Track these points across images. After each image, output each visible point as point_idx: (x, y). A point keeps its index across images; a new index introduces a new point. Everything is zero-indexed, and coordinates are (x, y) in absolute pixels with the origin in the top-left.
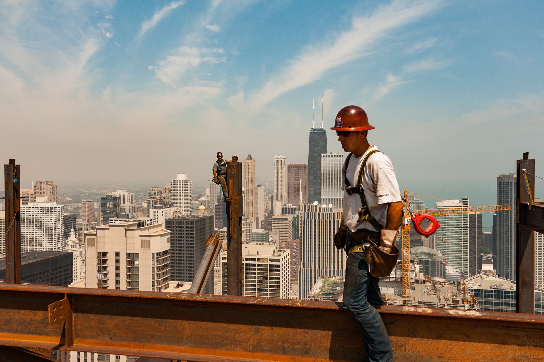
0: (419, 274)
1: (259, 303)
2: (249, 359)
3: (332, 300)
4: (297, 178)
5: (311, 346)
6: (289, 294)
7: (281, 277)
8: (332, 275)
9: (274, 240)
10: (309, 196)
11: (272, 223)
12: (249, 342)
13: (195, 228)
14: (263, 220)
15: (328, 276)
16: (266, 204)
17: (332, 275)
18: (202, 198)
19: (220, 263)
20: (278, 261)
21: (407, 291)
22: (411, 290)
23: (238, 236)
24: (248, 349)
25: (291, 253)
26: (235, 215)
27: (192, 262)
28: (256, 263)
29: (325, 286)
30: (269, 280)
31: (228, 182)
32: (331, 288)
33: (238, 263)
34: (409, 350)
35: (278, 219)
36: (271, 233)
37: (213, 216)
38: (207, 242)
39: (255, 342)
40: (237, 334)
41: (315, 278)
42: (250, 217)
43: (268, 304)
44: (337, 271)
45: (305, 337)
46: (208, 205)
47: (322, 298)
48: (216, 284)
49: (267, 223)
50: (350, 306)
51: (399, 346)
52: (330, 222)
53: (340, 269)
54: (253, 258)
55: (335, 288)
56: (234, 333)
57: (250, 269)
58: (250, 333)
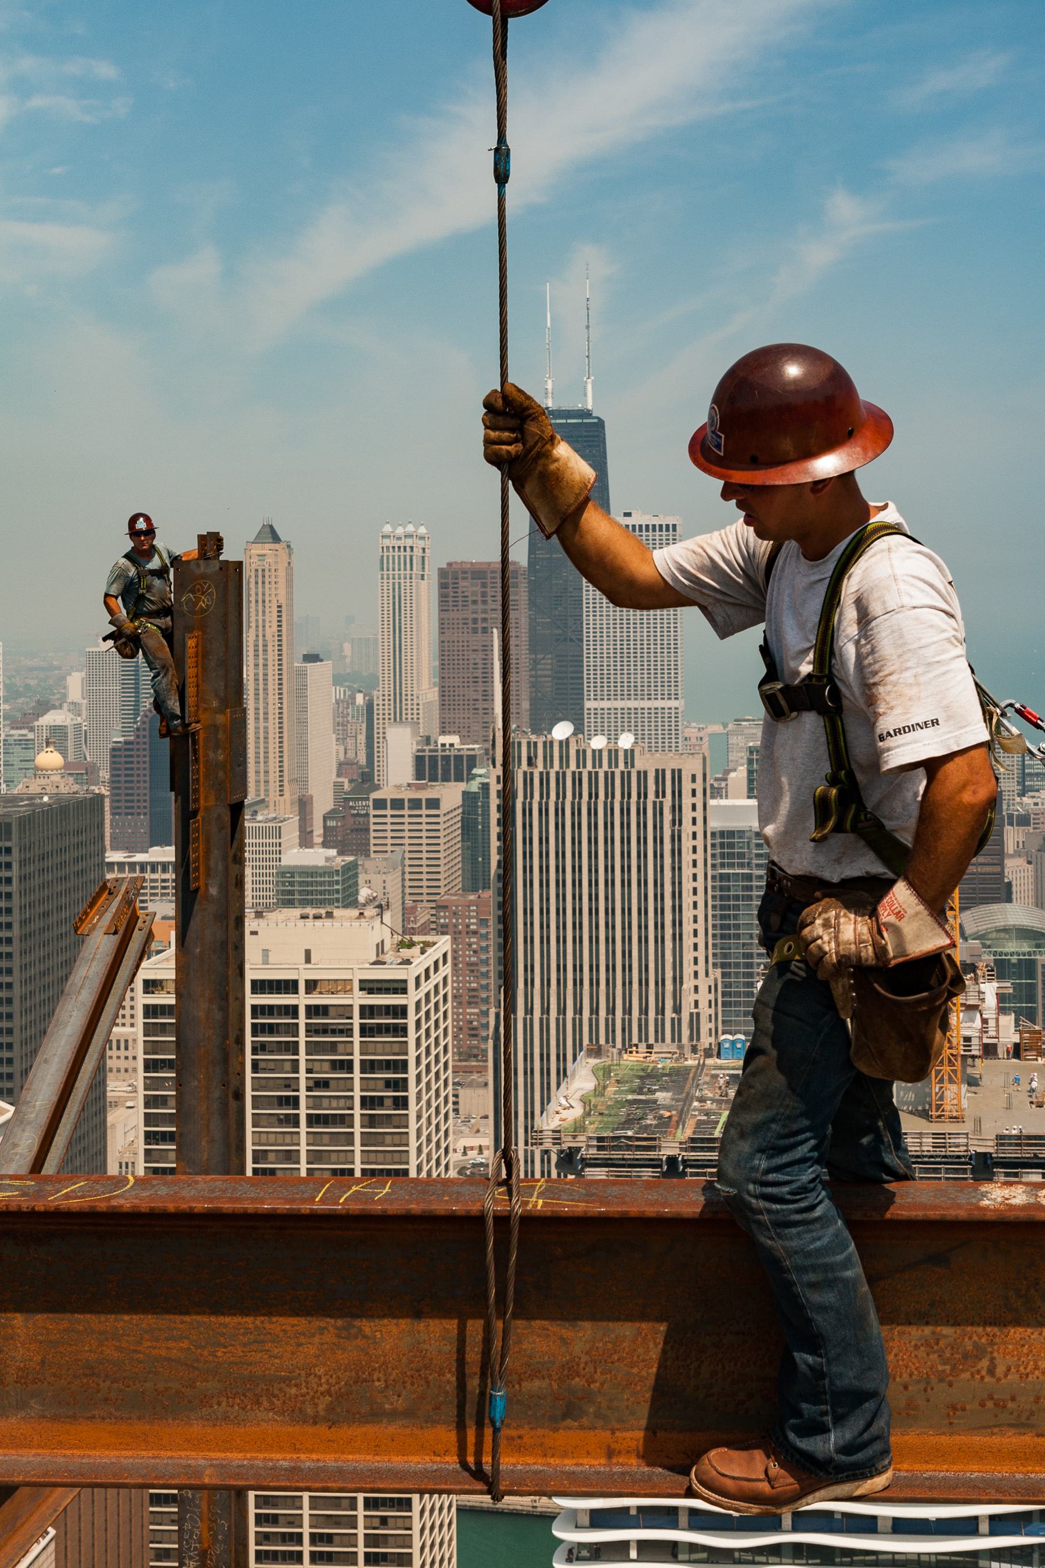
0: (997, 1020)
1: (356, 1207)
2: (314, 1456)
4: (480, 625)
5: (591, 1381)
6: (446, 1132)
8: (635, 1040)
9: (381, 896)
10: (533, 701)
11: (372, 820)
13: (15, 852)
14: (332, 811)
15: (619, 1045)
16: (341, 740)
17: (635, 1040)
18: (52, 718)
19: (132, 1008)
20: (399, 987)
21: (948, 1095)
22: (964, 1088)
23: (224, 888)
24: (310, 1410)
25: (455, 951)
26: (212, 797)
28: (302, 1000)
29: (605, 1087)
32: (630, 1097)
33: (224, 1009)
34: (1009, 1370)
35: (397, 804)
36: (368, 864)
37: (100, 797)
38: (81, 920)
40: (254, 1347)
41: (562, 1058)
42: (273, 796)
43: (395, 1208)
44: (656, 1020)
45: (564, 1341)
46: (78, 746)
47: (595, 1143)
49: (351, 820)
50: (751, 1187)
51: (966, 1356)
52: (625, 811)
53: (669, 1014)
54: (287, 982)
55: (651, 1097)
56: (245, 1345)
57: (271, 1029)
58: (316, 1340)
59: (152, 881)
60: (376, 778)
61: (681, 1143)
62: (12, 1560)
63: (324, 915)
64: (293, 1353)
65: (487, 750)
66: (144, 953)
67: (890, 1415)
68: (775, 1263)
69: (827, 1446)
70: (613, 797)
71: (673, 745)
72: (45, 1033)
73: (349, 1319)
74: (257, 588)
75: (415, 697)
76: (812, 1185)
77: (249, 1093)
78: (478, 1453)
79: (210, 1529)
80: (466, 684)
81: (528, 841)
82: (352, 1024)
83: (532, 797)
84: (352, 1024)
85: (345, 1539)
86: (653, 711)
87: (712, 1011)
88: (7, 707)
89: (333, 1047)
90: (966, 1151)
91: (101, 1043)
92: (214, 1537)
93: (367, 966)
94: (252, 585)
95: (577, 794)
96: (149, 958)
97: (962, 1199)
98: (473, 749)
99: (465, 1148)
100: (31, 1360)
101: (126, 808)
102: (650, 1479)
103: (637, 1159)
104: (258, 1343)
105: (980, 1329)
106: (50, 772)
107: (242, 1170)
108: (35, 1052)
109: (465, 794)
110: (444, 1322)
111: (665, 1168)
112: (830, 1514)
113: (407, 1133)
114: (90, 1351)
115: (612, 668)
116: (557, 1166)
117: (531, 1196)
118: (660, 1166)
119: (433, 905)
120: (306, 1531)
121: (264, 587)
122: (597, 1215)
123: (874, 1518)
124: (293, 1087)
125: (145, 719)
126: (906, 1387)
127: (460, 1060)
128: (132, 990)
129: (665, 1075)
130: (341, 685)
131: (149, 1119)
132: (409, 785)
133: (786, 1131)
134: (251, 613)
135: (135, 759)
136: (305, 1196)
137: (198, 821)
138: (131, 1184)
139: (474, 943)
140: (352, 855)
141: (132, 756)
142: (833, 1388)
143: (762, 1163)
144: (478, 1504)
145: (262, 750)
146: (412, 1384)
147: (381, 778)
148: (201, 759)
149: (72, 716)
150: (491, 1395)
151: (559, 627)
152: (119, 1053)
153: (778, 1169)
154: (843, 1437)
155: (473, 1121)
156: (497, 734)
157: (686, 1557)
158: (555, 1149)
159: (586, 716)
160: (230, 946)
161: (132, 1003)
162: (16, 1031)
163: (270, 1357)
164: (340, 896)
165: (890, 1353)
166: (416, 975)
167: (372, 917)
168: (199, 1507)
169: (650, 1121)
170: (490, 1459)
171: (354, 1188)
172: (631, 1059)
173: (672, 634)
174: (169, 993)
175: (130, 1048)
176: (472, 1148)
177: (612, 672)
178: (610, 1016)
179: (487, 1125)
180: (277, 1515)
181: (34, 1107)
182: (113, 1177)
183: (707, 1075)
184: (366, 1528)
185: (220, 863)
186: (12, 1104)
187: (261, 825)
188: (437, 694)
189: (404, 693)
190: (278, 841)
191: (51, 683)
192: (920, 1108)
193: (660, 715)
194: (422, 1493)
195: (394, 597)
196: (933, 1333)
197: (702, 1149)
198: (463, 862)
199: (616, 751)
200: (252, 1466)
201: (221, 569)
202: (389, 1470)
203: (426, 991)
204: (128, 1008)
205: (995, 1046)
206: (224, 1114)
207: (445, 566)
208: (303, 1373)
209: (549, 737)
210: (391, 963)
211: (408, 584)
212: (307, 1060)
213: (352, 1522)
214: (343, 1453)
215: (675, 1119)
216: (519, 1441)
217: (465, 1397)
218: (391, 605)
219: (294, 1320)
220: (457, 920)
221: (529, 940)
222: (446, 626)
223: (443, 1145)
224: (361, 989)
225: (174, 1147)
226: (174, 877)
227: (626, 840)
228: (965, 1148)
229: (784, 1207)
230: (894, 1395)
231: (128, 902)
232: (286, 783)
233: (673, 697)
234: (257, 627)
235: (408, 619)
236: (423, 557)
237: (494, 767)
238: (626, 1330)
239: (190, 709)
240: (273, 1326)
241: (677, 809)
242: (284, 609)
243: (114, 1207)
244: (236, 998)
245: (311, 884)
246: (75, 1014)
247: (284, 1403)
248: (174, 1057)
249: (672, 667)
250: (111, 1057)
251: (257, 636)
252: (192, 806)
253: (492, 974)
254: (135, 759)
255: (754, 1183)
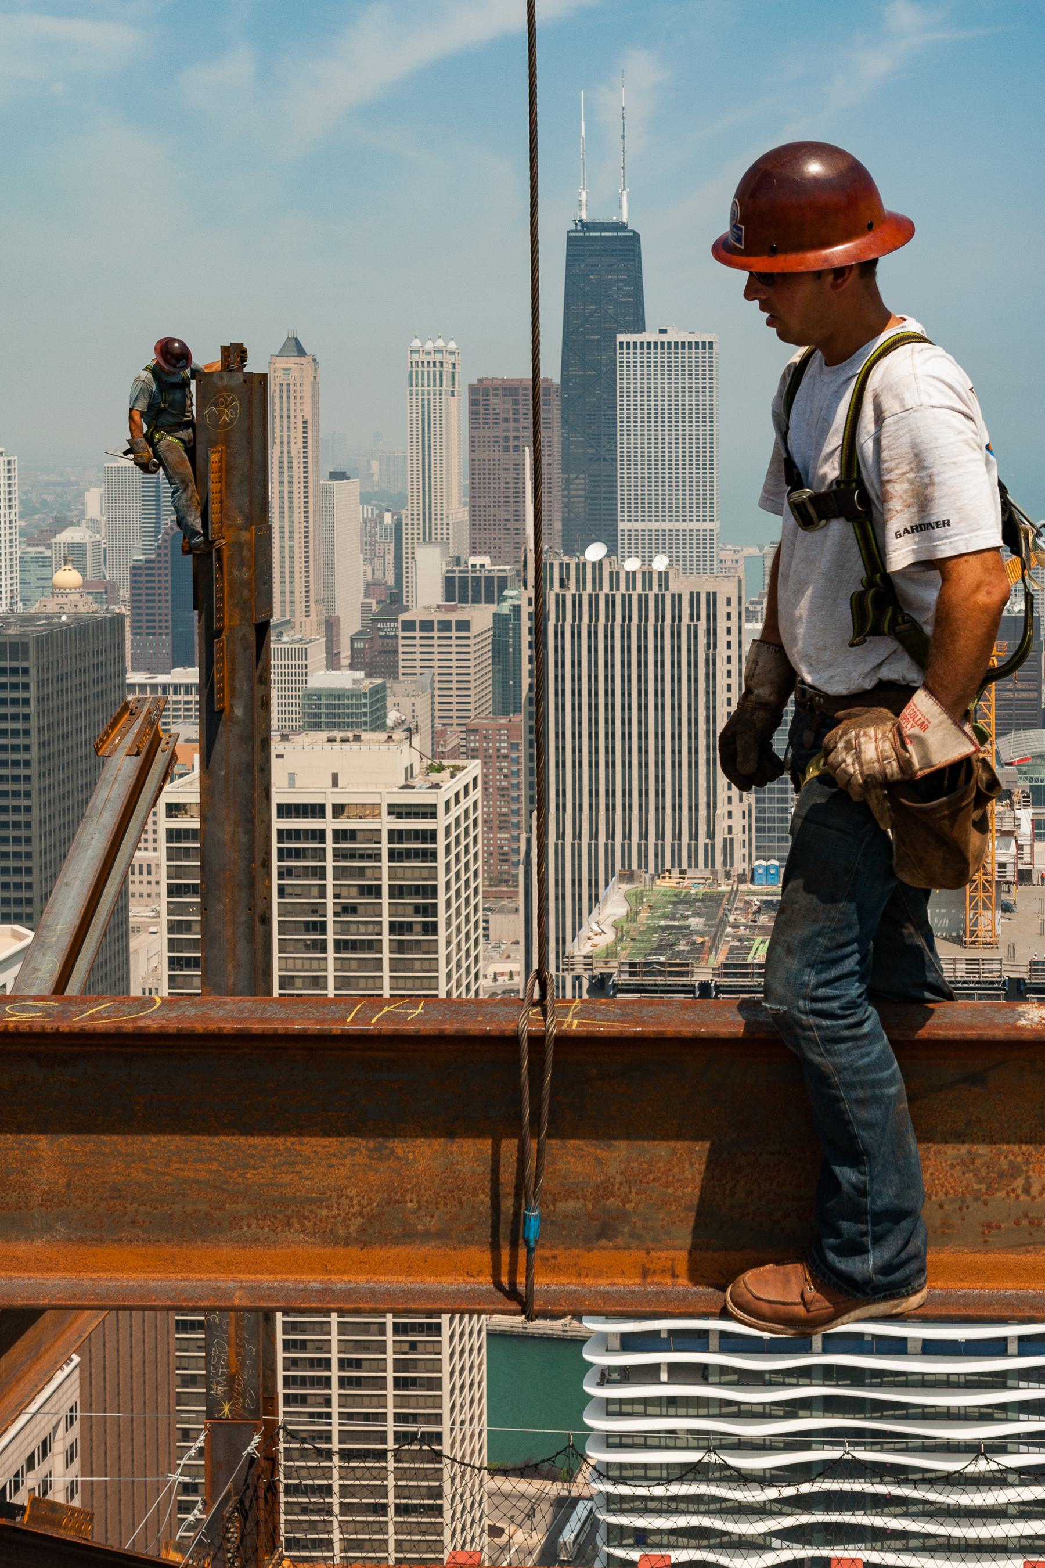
0: (1032, 846)
1: (388, 1028)
2: (346, 1278)
3: (671, 973)
4: (511, 443)
5: (625, 1201)
6: (476, 958)
7: (441, 883)
8: (668, 866)
9: (409, 719)
10: (566, 521)
11: (401, 642)
12: (344, 1201)
13: (33, 672)
15: (652, 870)
16: (369, 560)
17: (668, 866)
18: (70, 535)
19: (155, 832)
20: (428, 812)
21: (983, 920)
22: (998, 913)
23: (249, 709)
24: (341, 1232)
25: (485, 776)
26: (237, 616)
27: (22, 833)
28: (329, 824)
29: (637, 913)
30: (385, 900)
31: (199, 460)
32: (663, 923)
33: (250, 832)
35: (427, 626)
37: (121, 617)
38: (103, 742)
39: (371, 1201)
40: (284, 1168)
41: (593, 883)
42: (299, 617)
43: (428, 1028)
44: (689, 845)
45: (599, 1161)
46: (96, 564)
47: (627, 969)
48: (139, 930)
49: (379, 642)
50: (801, 1003)
51: (1001, 1175)
52: (659, 634)
53: (702, 839)
54: (313, 806)
56: (275, 1167)
57: (298, 854)
58: (348, 1161)
59: (175, 702)
60: (405, 599)
61: (713, 969)
62: (37, 1386)
63: (351, 739)
64: (324, 1175)
65: (518, 571)
66: (167, 776)
67: (926, 1234)
68: (822, 1078)
69: (865, 1266)
70: (647, 620)
71: (708, 567)
72: (65, 857)
73: (380, 1140)
74: (281, 403)
75: (444, 517)
76: (859, 1000)
77: (275, 919)
78: (513, 1273)
79: (238, 1354)
80: (497, 504)
81: (560, 664)
82: (380, 849)
83: (564, 620)
84: (380, 849)
85: (374, 1364)
86: (688, 533)
87: (746, 837)
88: (23, 523)
89: (361, 872)
90: (1000, 977)
91: (123, 867)
92: (242, 1363)
93: (396, 790)
94: (277, 400)
95: (610, 617)
96: (172, 781)
97: (999, 1019)
98: (504, 571)
99: (495, 974)
100: (56, 1183)
101: (148, 628)
102: (685, 1297)
103: (670, 985)
104: (289, 1164)
105: (1015, 1148)
106: (68, 591)
107: (269, 992)
108: (54, 877)
109: (496, 616)
110: (479, 1141)
111: (698, 994)
112: (860, 1336)
113: (437, 959)
114: (117, 1173)
115: (646, 488)
116: (589, 992)
117: (566, 1016)
118: (693, 992)
119: (464, 728)
120: (335, 1356)
121: (289, 403)
122: (633, 1034)
123: (904, 1340)
124: (320, 913)
125: (166, 537)
126: (941, 1206)
127: (490, 886)
128: (155, 814)
129: (698, 901)
130: (369, 504)
131: (172, 945)
132: (439, 606)
133: (834, 944)
134: (276, 429)
135: (156, 578)
136: (337, 1016)
137: (222, 641)
138: (158, 1005)
139: (505, 767)
140: (380, 677)
141: (153, 575)
142: (874, 1207)
143: (811, 978)
144: (508, 1329)
145: (287, 570)
146: (445, 1205)
147: (410, 599)
148: (226, 578)
149: (90, 533)
150: (525, 1215)
151: (592, 446)
152: (142, 878)
153: (827, 983)
154: (882, 1257)
155: (503, 947)
156: (529, 555)
157: (716, 1379)
158: (586, 975)
159: (619, 537)
160: (256, 768)
161: (155, 827)
162: (36, 856)
163: (301, 1178)
164: (368, 719)
165: (926, 1172)
166: (446, 799)
167: (401, 741)
168: (225, 1332)
169: (682, 946)
170: (524, 1280)
171: (386, 1009)
172: (663, 885)
173: (708, 454)
174: (192, 817)
175: (153, 873)
176: (502, 974)
177: (646, 492)
178: (643, 842)
179: (517, 951)
180: (305, 1341)
181: (55, 930)
182: (136, 999)
183: (740, 901)
184: (395, 1353)
185: (245, 684)
186: (31, 929)
187: (286, 646)
188: (467, 514)
189: (433, 513)
190: (304, 662)
191: (69, 498)
192: (954, 934)
193: (695, 537)
194: (453, 1312)
195: (423, 413)
196: (969, 1152)
197: (735, 975)
198: (493, 684)
199: (650, 573)
200: (283, 1288)
201: (245, 381)
202: (422, 1291)
203: (456, 815)
204: (150, 832)
205: (1030, 872)
206: (251, 938)
207: (476, 382)
208: (334, 1194)
209: (582, 558)
210: (421, 788)
211: (438, 400)
212: (334, 885)
213: (381, 1347)
214: (375, 1274)
215: (708, 944)
216: (553, 1261)
217: (499, 1218)
218: (420, 422)
219: (326, 1141)
220: (488, 743)
221: (561, 765)
222: (477, 444)
223: (473, 971)
224: (390, 814)
225: (200, 973)
226: (197, 698)
227: (659, 664)
228: (998, 974)
229: (834, 1023)
230: (930, 1214)
231: (151, 723)
232: (312, 604)
233: (708, 518)
234: (282, 443)
235: (438, 436)
236: (453, 373)
237: (526, 588)
238: (662, 1149)
239: (213, 526)
240: (304, 1148)
241: (712, 632)
242: (309, 425)
243: (142, 1028)
244: (263, 822)
245: (338, 706)
246: (96, 836)
247: (315, 1224)
248: (199, 882)
249: (708, 488)
250: (133, 882)
251: (282, 452)
252: (216, 625)
253: (523, 799)
254: (156, 578)
255: (805, 999)
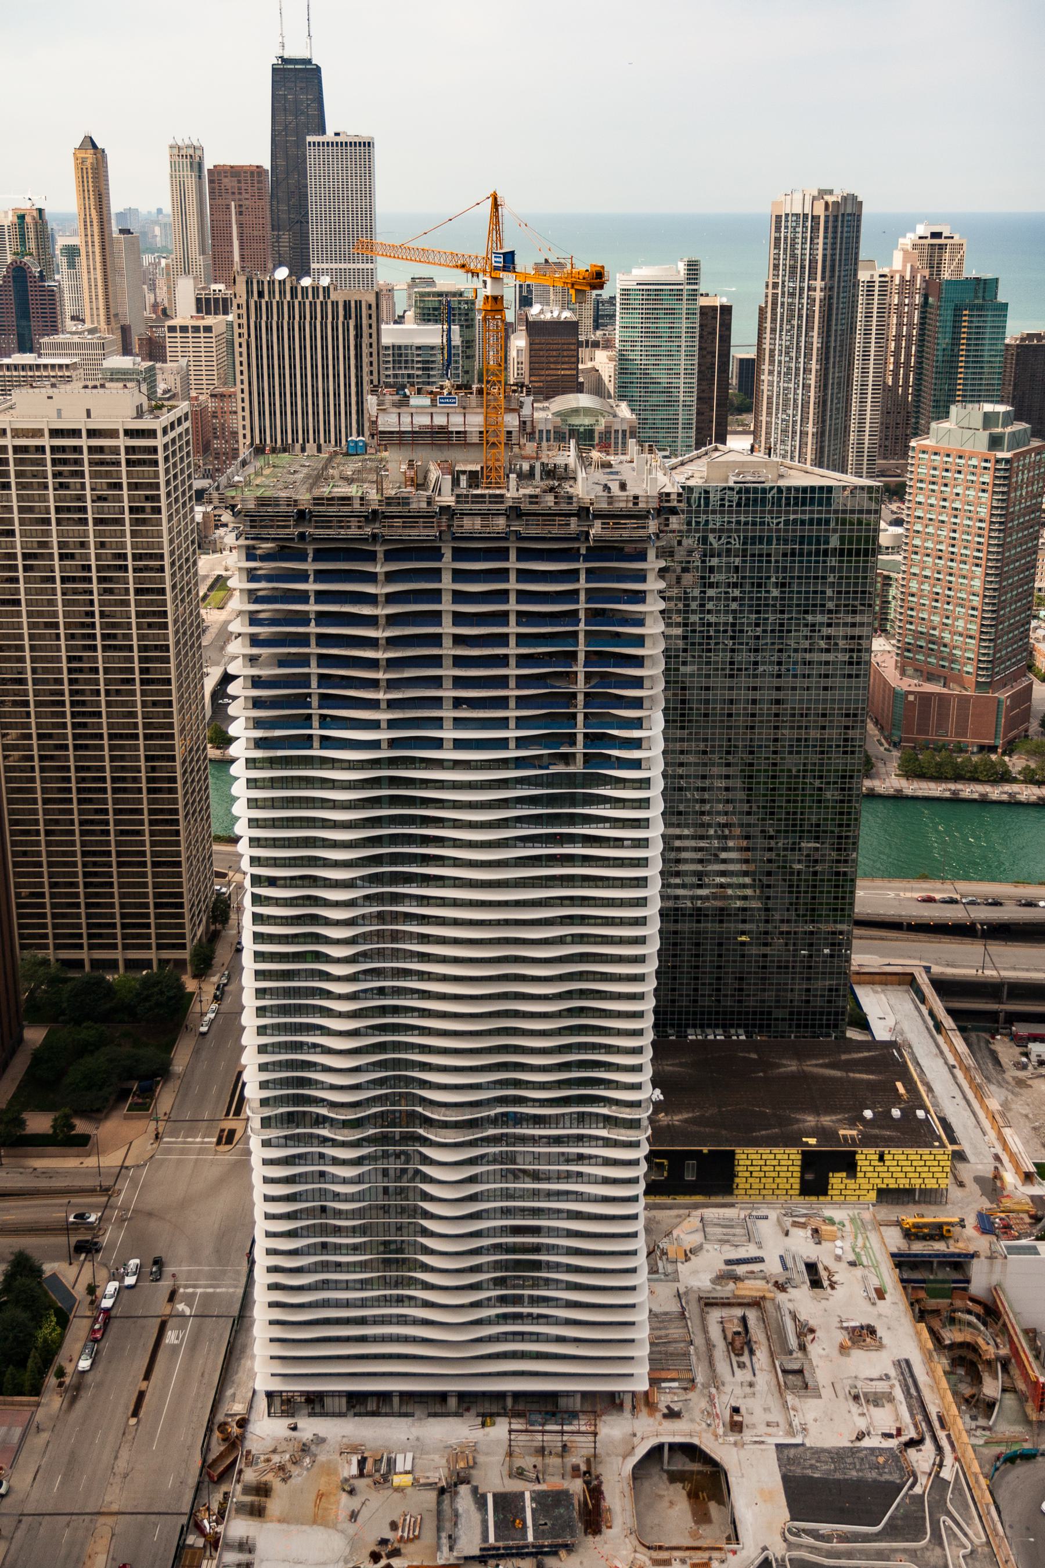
20: (151, 434)
28: (84, 442)
30: (125, 492)
35: (184, 329)
57: (65, 462)
